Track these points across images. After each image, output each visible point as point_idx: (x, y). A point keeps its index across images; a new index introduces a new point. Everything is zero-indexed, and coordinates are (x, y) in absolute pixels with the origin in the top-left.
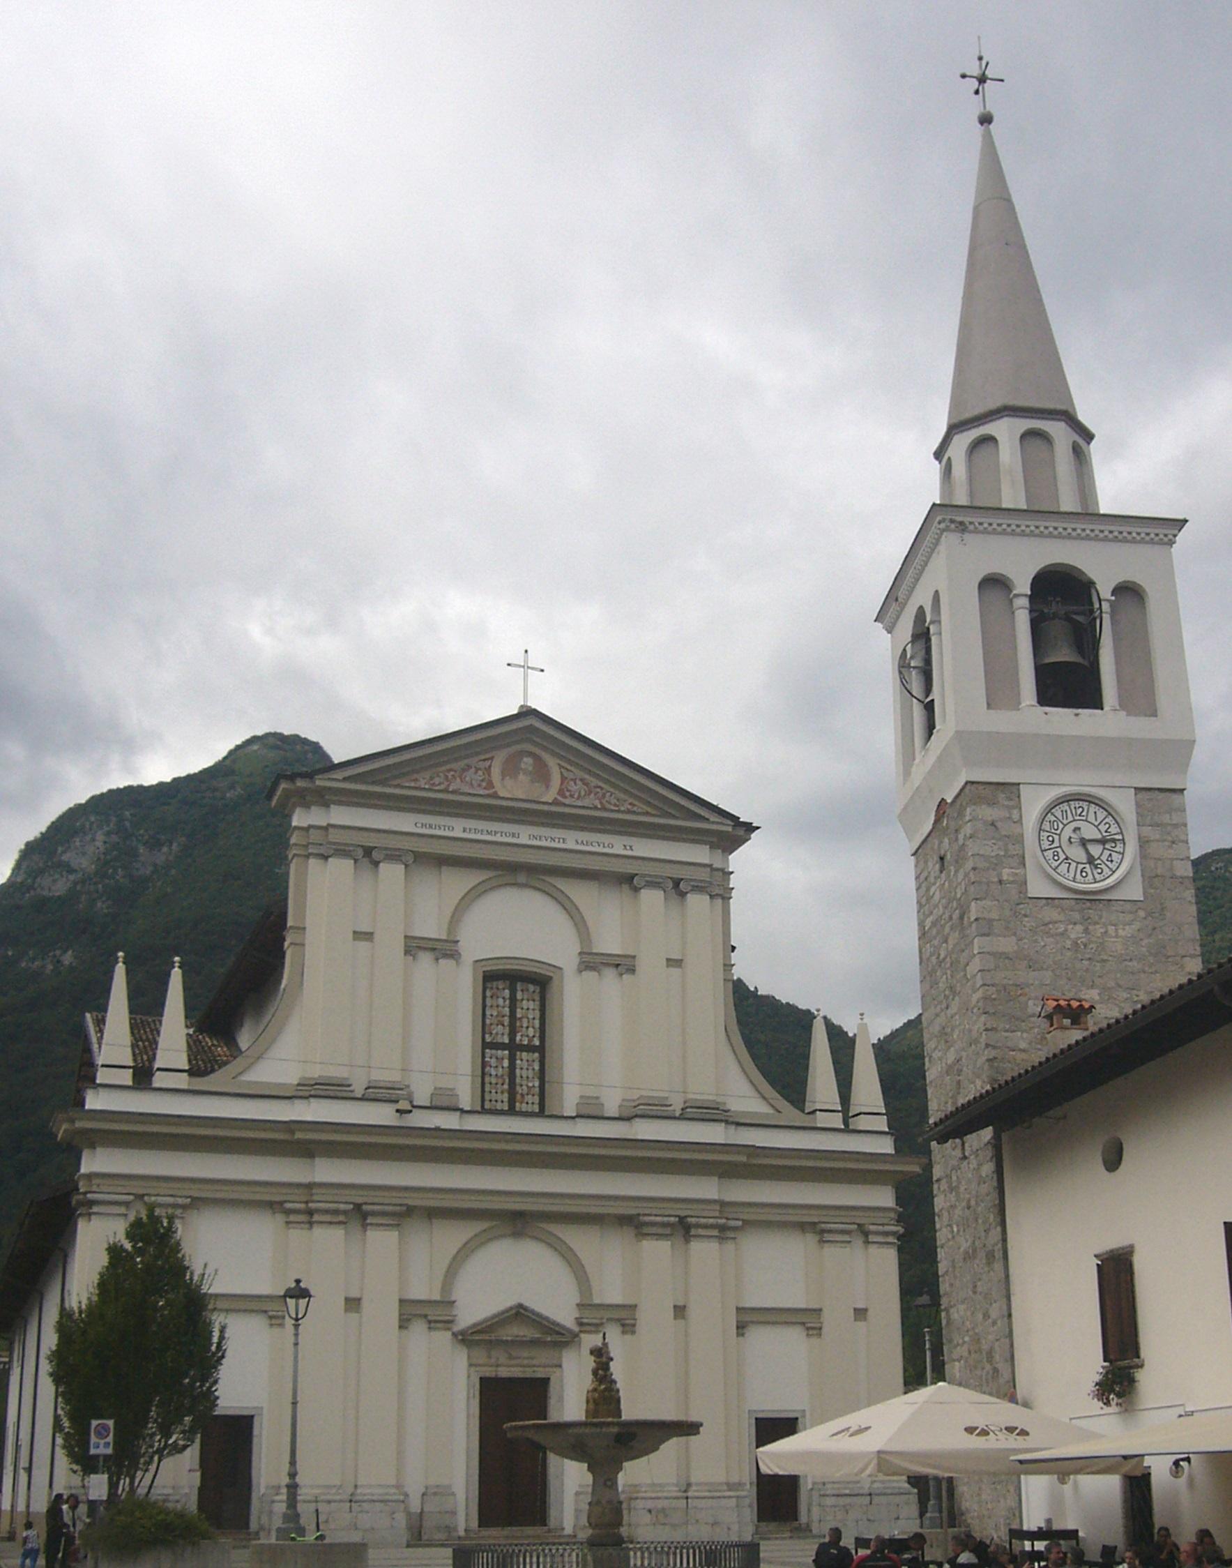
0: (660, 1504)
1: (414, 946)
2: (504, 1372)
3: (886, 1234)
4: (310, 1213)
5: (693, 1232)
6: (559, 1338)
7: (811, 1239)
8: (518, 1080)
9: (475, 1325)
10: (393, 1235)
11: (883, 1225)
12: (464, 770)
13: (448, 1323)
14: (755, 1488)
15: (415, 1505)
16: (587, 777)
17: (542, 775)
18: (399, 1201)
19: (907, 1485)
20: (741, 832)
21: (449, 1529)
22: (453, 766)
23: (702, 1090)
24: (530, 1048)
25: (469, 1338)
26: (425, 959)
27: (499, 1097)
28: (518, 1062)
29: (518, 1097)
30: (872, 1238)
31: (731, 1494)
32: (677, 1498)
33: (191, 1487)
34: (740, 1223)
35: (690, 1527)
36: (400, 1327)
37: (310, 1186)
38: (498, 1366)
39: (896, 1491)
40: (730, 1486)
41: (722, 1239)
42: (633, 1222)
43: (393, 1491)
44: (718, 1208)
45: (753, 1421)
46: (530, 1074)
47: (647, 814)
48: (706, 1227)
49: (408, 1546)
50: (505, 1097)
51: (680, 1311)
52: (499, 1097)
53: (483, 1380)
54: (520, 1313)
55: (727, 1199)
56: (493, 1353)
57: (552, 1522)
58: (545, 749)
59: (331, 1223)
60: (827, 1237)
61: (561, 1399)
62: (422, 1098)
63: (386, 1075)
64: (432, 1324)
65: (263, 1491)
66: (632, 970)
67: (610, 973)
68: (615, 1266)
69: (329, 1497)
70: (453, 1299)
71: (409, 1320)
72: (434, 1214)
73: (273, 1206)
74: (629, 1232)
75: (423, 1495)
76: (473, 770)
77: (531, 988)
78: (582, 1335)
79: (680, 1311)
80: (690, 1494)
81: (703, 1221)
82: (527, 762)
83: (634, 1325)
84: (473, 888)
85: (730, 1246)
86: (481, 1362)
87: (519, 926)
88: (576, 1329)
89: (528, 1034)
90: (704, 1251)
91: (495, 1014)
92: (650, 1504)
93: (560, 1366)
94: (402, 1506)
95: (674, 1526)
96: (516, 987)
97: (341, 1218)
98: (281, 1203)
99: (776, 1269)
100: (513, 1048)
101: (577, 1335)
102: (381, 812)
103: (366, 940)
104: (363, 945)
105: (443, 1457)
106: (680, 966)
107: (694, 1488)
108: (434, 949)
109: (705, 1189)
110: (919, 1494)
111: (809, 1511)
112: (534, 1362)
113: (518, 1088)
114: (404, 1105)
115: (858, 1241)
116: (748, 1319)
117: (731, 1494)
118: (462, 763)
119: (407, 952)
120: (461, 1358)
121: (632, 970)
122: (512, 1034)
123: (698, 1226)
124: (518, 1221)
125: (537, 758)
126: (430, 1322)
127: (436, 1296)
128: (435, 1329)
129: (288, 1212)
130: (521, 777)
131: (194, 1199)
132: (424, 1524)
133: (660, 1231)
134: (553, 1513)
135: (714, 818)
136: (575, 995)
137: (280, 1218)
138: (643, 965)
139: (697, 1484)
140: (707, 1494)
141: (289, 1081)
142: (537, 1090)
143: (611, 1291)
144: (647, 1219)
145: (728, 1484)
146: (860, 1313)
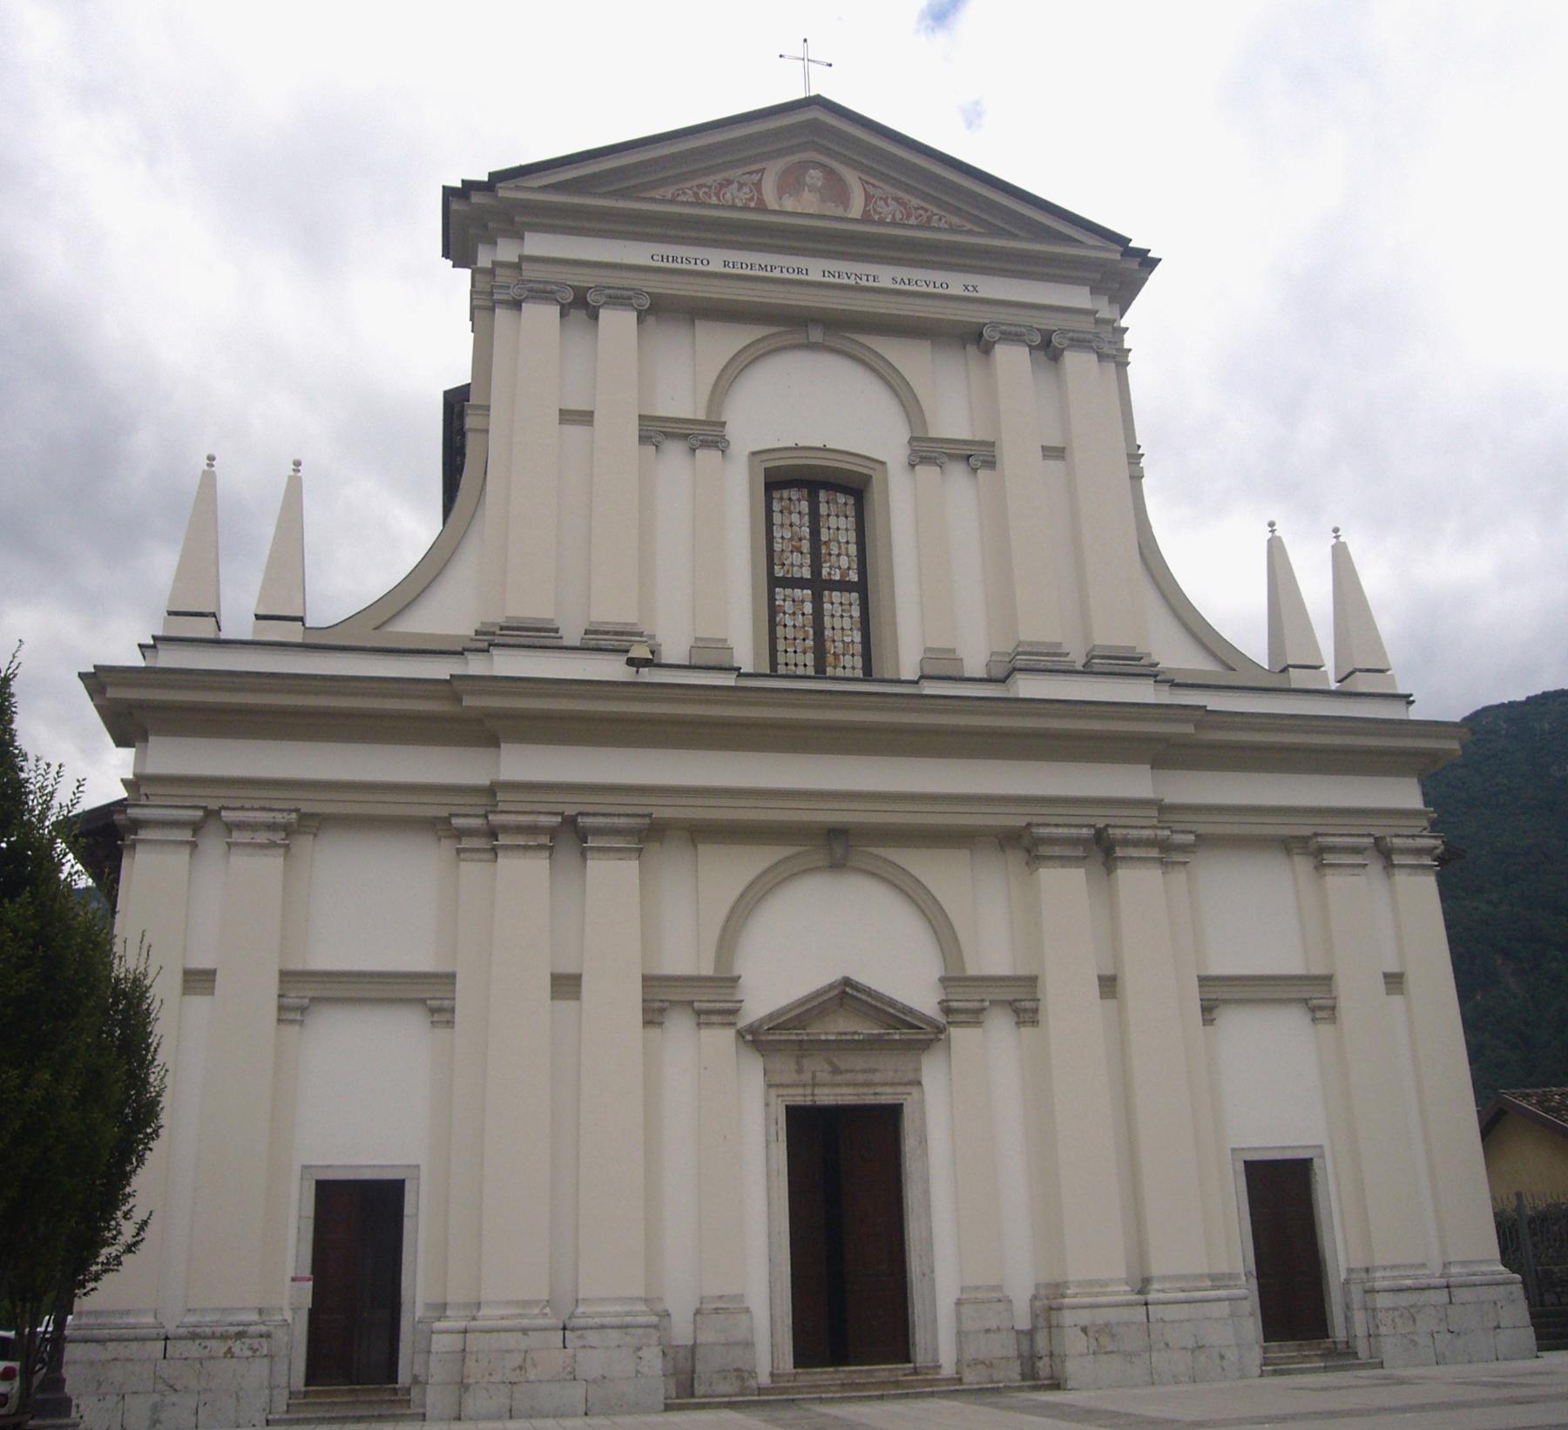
0: (1102, 1316)
1: (656, 432)
2: (827, 1097)
3: (1419, 852)
4: (493, 833)
5: (1119, 852)
6: (908, 1034)
7: (1303, 865)
8: (828, 633)
9: (771, 1017)
10: (631, 867)
11: (1413, 836)
12: (721, 186)
13: (729, 1014)
14: (1254, 1283)
15: (682, 1332)
16: (900, 194)
17: (839, 192)
18: (640, 810)
19: (1502, 1268)
20: (1133, 264)
21: (742, 1375)
22: (709, 180)
23: (1111, 635)
24: (843, 586)
25: (763, 1039)
26: (675, 452)
27: (800, 658)
28: (827, 606)
29: (830, 659)
30: (1397, 859)
31: (1222, 1293)
32: (1129, 1304)
33: (295, 1310)
34: (1191, 838)
35: (1155, 1355)
36: (647, 1023)
37: (492, 790)
38: (814, 1085)
39: (1489, 1278)
40: (1217, 1280)
41: (1164, 864)
42: (1021, 841)
43: (642, 1307)
44: (1155, 813)
45: (1241, 1167)
46: (847, 623)
47: (970, 232)
48: (1137, 843)
49: (668, 1408)
50: (810, 659)
51: (1109, 985)
52: (800, 658)
53: (791, 1111)
54: (847, 995)
55: (1167, 801)
56: (806, 1062)
57: (921, 1357)
58: (836, 156)
59: (526, 848)
60: (1329, 858)
61: (923, 1141)
62: (674, 651)
63: (613, 610)
64: (704, 1017)
65: (419, 1313)
66: (990, 463)
67: (957, 471)
68: (992, 911)
69: (525, 1322)
70: (736, 973)
71: (662, 1011)
72: (701, 833)
73: (440, 827)
74: (1015, 858)
75: (698, 1312)
76: (735, 185)
77: (841, 499)
78: (954, 1032)
79: (1109, 985)
80: (1152, 1297)
81: (1134, 833)
82: (814, 176)
83: (1036, 1011)
84: (733, 359)
85: (1178, 877)
86: (786, 1079)
87: (814, 405)
88: (941, 1019)
89: (840, 564)
90: (1138, 882)
91: (788, 535)
92: (1085, 1317)
93: (919, 1083)
94: (655, 1334)
95: (1129, 1356)
96: (818, 490)
97: (544, 840)
98: (446, 820)
99: (1252, 915)
100: (818, 586)
101: (940, 1030)
102: (598, 241)
103: (582, 423)
104: (576, 432)
105: (735, 1247)
106: (1063, 458)
107: (1156, 1286)
108: (686, 436)
109: (1131, 782)
110: (1524, 1283)
111: (1347, 1319)
112: (877, 1077)
113: (829, 645)
114: (640, 652)
115: (1376, 867)
116: (1218, 995)
117: (1222, 1293)
118: (720, 177)
119: (644, 439)
120: (753, 1072)
121: (990, 463)
122: (816, 566)
123: (1126, 842)
124: (837, 843)
125: (830, 172)
126: (699, 1013)
127: (707, 970)
128: (708, 1024)
129: (460, 834)
130: (806, 194)
131: (304, 817)
132: (698, 1368)
133: (1068, 852)
134: (920, 1336)
135: (1091, 240)
136: (903, 500)
137: (448, 846)
138: (1008, 457)
139: (1164, 1278)
140: (1182, 1295)
141: (461, 632)
142: (858, 648)
143: (992, 954)
144: (1043, 831)
145: (1213, 1277)
146: (1394, 981)
